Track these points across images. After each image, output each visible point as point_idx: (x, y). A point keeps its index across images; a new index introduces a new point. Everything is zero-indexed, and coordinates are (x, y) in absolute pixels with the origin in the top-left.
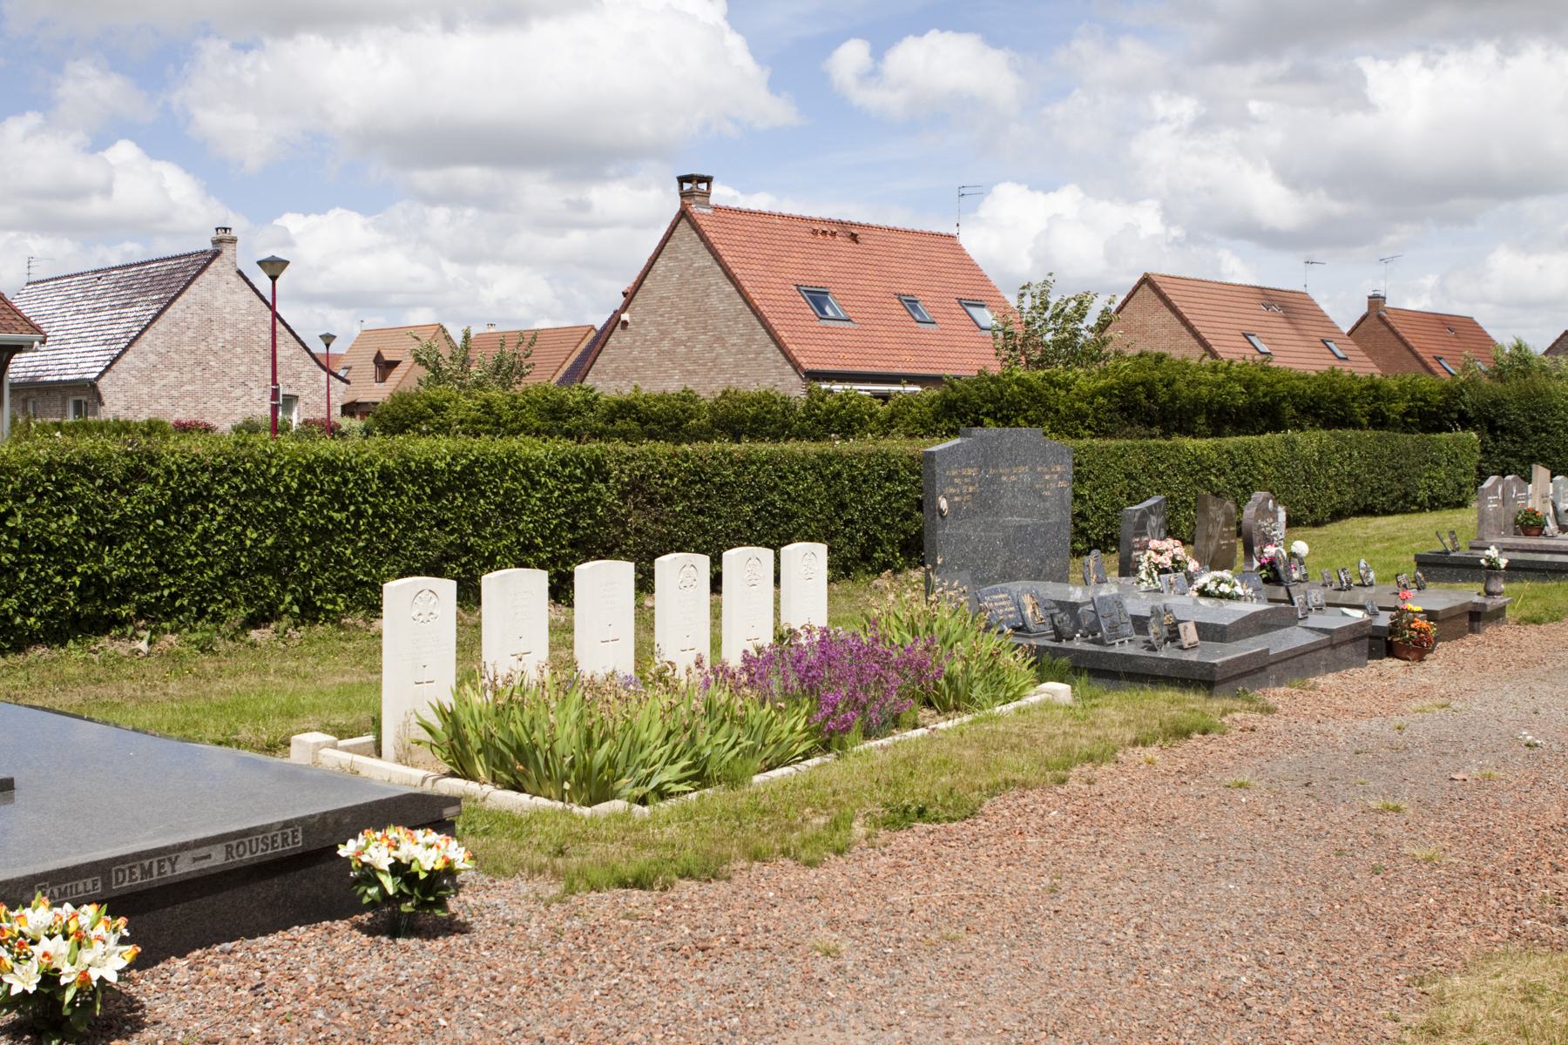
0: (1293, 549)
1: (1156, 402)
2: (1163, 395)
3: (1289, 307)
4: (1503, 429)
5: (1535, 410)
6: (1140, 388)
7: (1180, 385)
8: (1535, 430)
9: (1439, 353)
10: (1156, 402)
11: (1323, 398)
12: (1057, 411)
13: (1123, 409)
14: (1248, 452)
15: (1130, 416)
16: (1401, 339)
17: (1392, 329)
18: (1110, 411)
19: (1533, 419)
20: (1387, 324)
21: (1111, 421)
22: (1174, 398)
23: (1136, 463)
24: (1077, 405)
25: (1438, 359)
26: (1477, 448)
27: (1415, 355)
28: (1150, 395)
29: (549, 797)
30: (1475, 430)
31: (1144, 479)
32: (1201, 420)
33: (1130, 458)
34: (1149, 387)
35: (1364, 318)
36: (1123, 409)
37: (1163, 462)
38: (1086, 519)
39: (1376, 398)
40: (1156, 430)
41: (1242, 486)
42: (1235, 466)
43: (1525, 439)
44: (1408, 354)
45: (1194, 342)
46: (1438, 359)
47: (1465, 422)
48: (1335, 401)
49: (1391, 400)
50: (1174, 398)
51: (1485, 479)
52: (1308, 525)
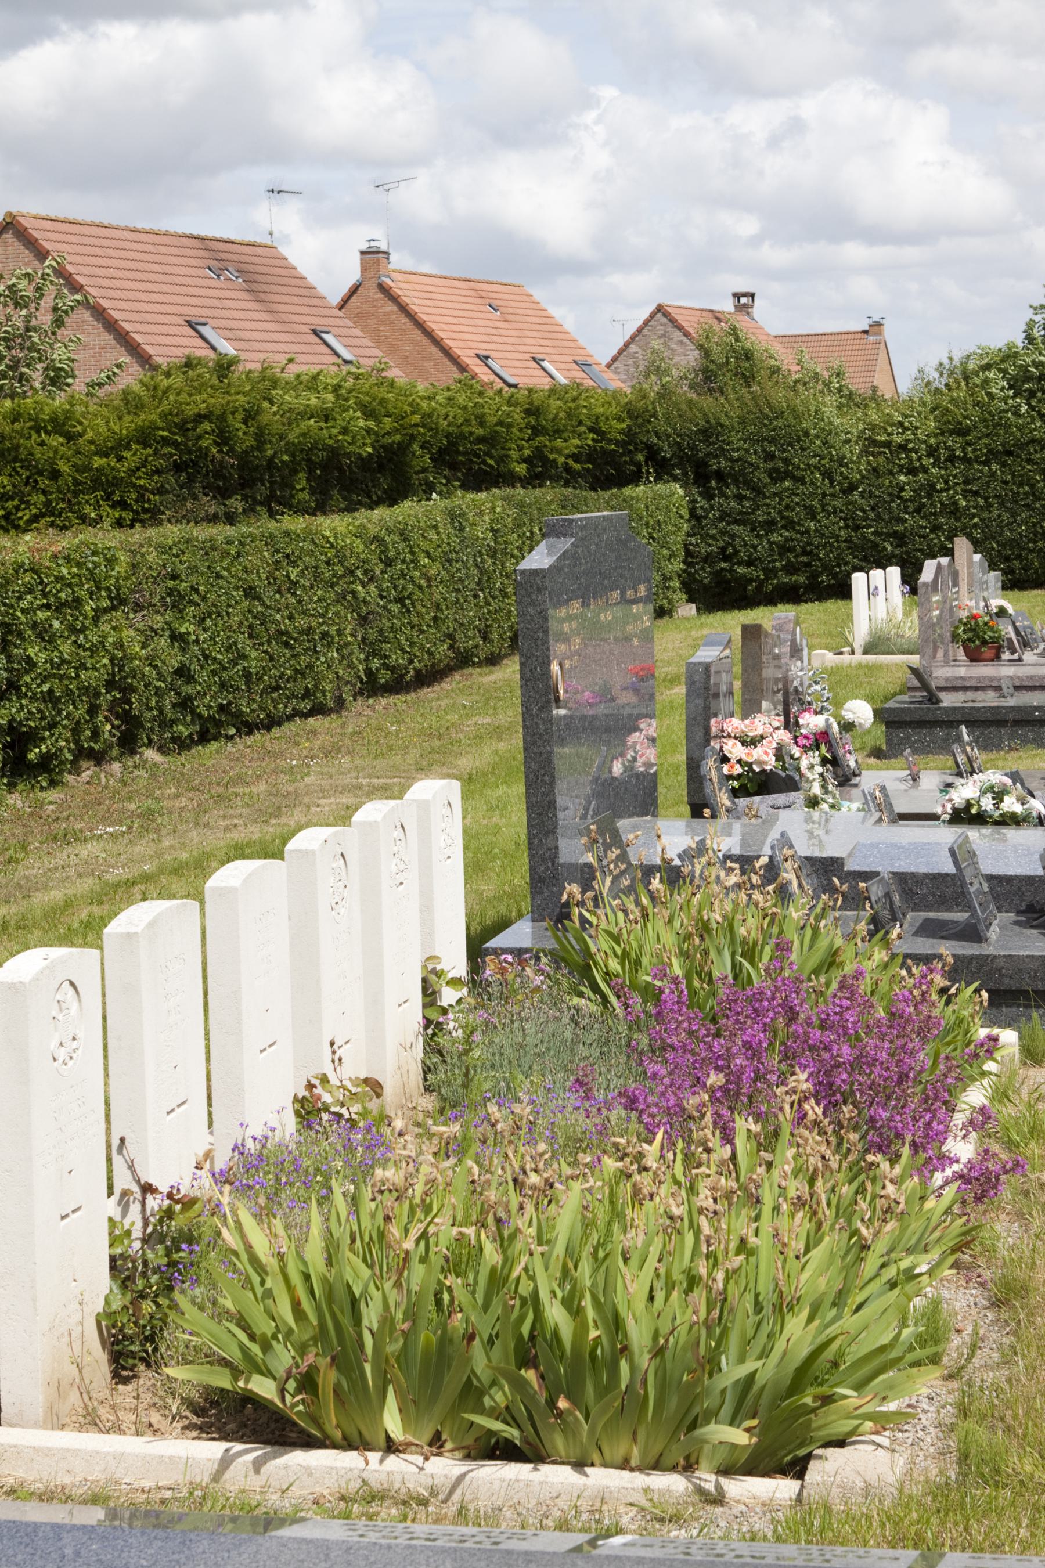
0: (849, 716)
1: (231, 452)
2: (244, 437)
3: (250, 270)
4: (720, 476)
5: (773, 441)
6: (206, 426)
7: (270, 413)
8: (776, 476)
9: (484, 349)
10: (231, 452)
11: (462, 436)
12: (55, 475)
13: (178, 468)
14: (404, 537)
15: (191, 479)
16: (420, 325)
17: (403, 309)
18: (158, 472)
19: (770, 457)
20: (394, 299)
21: (161, 491)
22: (261, 438)
23: (259, 563)
24: (98, 462)
25: (484, 359)
26: (685, 512)
27: (447, 352)
28: (224, 438)
29: (624, 1465)
30: (675, 479)
31: (269, 594)
32: (301, 481)
33: (250, 560)
34: (219, 419)
35: (354, 290)
36: (178, 468)
37: (294, 564)
38: (190, 679)
39: (536, 431)
40: (236, 504)
41: (400, 600)
42: (389, 563)
43: (758, 491)
44: (434, 350)
45: (108, 338)
46: (484, 359)
47: (663, 469)
48: (481, 440)
49: (558, 432)
50: (261, 438)
51: (920, 570)
52: (480, 664)
